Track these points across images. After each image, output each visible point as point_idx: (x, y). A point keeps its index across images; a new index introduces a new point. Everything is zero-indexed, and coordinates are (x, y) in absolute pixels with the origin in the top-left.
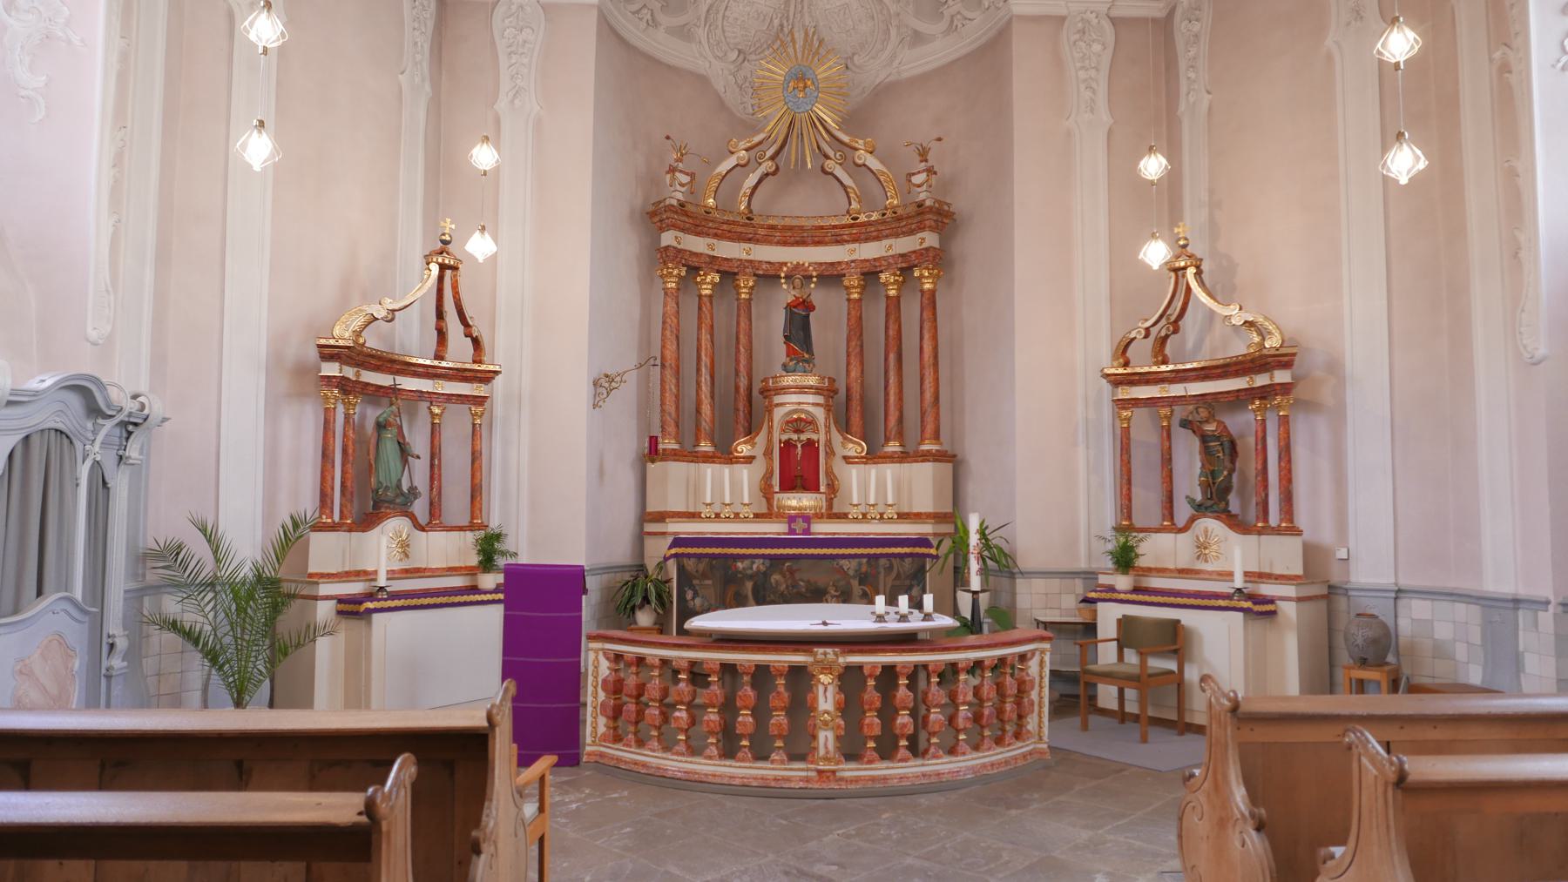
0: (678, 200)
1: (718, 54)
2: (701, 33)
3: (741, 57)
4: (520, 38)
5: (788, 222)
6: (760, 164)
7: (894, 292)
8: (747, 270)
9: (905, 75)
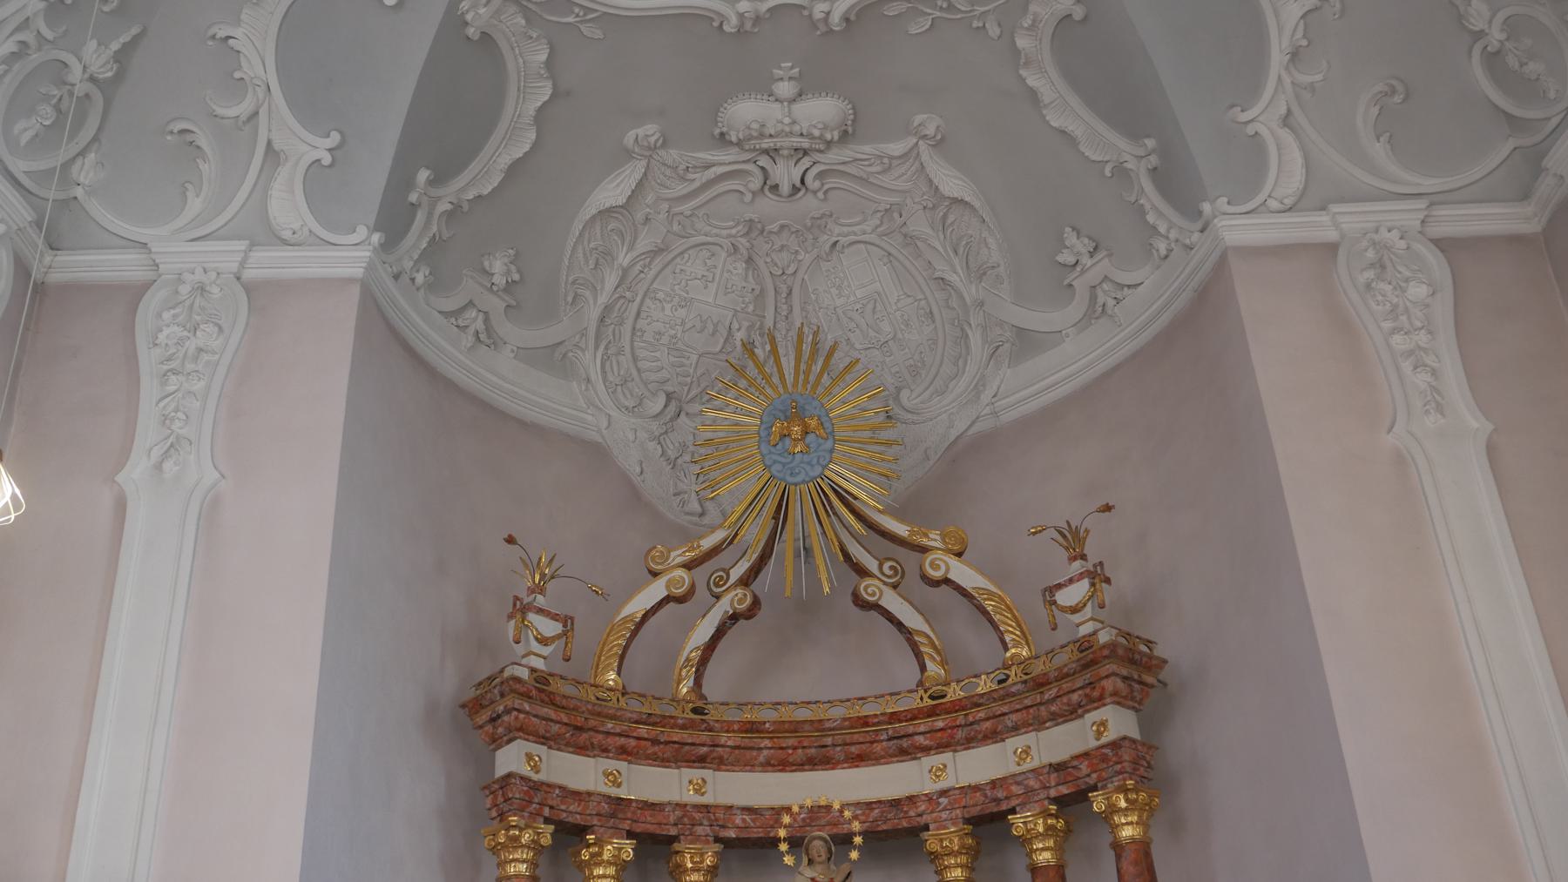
0: (533, 670)
1: (627, 403)
2: (590, 361)
3: (672, 408)
4: (191, 345)
5: (786, 714)
6: (718, 597)
7: (1047, 855)
8: (699, 830)
9: (1008, 417)
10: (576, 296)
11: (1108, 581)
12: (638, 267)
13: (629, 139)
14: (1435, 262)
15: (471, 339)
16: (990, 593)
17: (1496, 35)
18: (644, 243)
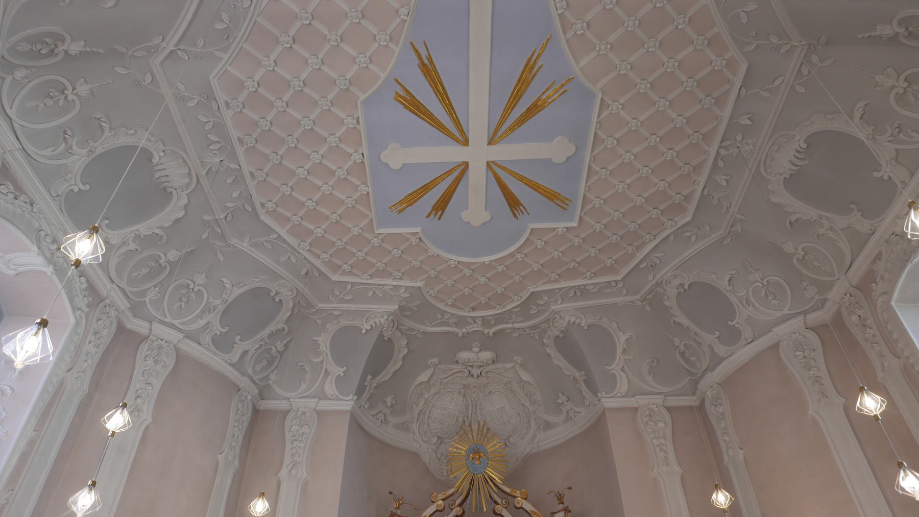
3: (440, 441)
4: (301, 431)
6: (452, 509)
10: (411, 407)
11: (570, 511)
12: (430, 398)
13: (429, 362)
14: (667, 415)
15: (380, 422)
16: (535, 513)
17: (682, 348)
18: (433, 391)
